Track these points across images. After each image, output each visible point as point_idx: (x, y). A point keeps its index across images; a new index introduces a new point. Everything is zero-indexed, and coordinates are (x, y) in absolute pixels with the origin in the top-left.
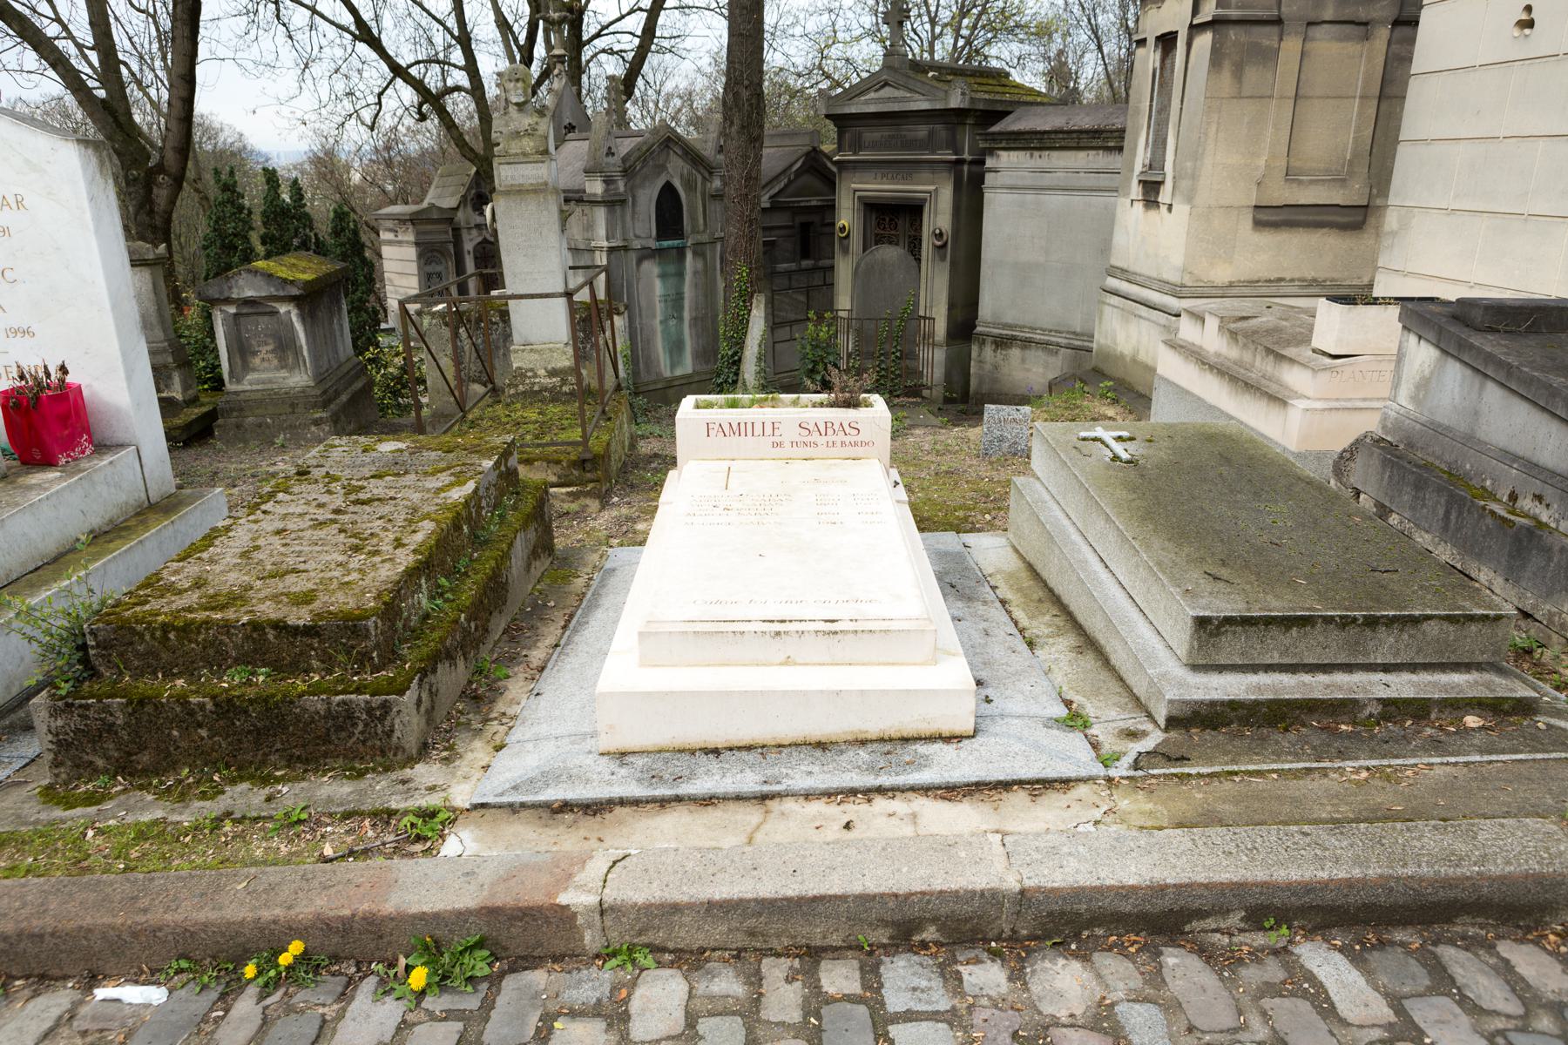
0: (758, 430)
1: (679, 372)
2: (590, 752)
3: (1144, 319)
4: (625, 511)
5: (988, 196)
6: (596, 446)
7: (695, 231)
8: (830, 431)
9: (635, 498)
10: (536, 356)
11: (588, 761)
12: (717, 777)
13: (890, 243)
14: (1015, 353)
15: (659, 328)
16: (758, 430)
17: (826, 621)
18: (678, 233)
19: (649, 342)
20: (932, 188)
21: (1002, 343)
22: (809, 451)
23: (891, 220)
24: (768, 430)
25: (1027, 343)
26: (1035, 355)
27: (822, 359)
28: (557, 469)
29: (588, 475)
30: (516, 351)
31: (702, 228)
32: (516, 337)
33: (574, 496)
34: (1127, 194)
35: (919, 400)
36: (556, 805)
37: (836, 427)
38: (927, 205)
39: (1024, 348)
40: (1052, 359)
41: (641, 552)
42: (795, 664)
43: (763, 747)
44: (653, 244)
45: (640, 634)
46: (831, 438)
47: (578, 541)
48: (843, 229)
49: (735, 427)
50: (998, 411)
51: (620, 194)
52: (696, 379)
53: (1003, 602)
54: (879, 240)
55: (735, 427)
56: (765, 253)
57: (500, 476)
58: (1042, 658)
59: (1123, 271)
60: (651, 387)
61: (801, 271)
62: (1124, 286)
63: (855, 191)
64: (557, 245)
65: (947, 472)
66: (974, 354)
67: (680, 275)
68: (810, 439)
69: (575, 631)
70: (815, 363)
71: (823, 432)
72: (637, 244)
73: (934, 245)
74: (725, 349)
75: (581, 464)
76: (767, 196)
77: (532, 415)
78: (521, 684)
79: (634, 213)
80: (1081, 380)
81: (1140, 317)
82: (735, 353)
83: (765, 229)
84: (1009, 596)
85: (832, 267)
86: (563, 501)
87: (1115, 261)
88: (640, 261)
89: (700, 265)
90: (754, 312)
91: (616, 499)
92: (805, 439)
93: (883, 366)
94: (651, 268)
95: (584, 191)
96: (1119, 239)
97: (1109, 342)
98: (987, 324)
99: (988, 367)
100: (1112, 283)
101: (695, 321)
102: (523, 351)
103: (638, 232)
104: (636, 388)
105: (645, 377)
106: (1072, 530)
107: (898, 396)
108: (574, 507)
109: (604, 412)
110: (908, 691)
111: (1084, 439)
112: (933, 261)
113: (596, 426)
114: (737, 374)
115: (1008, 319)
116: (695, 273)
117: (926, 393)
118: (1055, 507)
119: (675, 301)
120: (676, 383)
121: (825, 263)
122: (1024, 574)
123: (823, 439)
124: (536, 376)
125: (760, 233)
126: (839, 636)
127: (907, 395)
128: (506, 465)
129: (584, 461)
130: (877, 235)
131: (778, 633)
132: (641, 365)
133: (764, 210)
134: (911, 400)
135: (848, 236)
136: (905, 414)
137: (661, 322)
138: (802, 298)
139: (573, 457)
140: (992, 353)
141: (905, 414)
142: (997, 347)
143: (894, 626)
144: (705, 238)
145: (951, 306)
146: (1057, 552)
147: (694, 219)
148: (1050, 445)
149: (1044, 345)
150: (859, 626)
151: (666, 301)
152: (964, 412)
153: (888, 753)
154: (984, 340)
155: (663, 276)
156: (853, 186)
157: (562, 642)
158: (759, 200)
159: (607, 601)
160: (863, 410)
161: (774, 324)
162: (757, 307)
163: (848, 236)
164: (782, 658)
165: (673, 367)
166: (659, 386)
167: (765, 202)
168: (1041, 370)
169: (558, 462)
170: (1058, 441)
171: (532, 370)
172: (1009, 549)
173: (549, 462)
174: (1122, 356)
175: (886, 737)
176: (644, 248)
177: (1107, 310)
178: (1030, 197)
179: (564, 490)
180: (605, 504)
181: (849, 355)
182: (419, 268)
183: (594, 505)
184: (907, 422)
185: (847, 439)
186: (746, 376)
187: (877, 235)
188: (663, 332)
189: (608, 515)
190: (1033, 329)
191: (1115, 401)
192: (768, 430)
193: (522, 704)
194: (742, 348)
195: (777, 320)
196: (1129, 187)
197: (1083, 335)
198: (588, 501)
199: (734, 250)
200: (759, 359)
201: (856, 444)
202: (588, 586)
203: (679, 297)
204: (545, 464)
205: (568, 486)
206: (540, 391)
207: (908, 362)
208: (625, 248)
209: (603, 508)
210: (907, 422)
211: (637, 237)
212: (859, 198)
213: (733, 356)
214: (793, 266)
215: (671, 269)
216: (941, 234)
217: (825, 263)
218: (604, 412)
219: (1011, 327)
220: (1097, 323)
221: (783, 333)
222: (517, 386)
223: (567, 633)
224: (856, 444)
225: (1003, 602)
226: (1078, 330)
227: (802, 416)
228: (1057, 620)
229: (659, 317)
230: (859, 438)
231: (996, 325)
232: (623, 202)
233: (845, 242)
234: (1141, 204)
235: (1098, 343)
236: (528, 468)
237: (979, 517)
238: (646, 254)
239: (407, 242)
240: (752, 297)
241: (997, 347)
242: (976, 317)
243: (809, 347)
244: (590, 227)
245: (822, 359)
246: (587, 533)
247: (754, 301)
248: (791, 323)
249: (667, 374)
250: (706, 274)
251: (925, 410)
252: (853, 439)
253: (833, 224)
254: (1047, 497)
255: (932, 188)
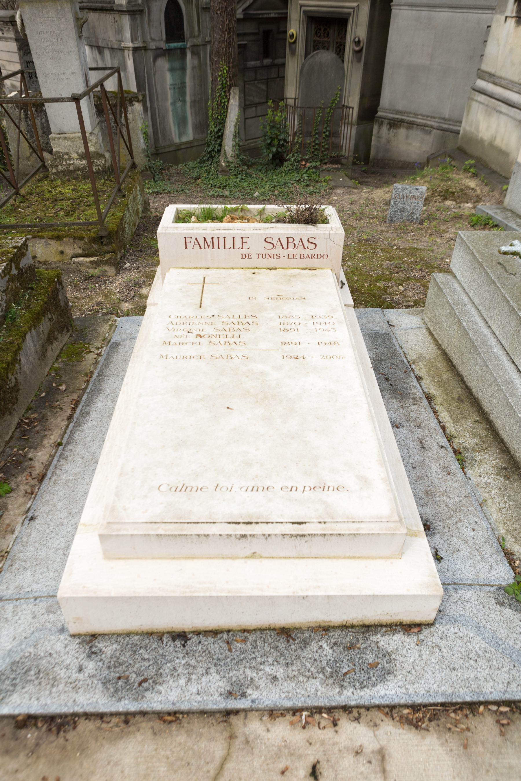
0: (229, 243)
1: (184, 139)
2: (62, 630)
3: (504, 114)
4: (134, 275)
5: (394, 12)
6: (111, 223)
7: (192, 36)
8: (291, 245)
9: (143, 262)
10: (69, 143)
11: (59, 646)
12: (182, 681)
13: (324, 48)
14: (402, 131)
15: (170, 108)
16: (229, 243)
17: (293, 523)
18: (181, 38)
19: (164, 118)
20: (355, 4)
21: (394, 124)
22: (273, 262)
23: (325, 30)
24: (238, 244)
25: (411, 125)
26: (416, 134)
27: (277, 136)
28: (81, 244)
29: (106, 248)
30: (54, 139)
31: (197, 33)
32: (53, 128)
33: (96, 264)
34: (503, 12)
35: (339, 166)
36: (20, 718)
37: (297, 242)
38: (351, 18)
39: (408, 128)
40: (427, 137)
41: (139, 324)
42: (261, 557)
43: (229, 631)
44: (164, 45)
45: (101, 536)
46: (291, 251)
47: (98, 304)
48: (292, 36)
49: (209, 240)
50: (403, 189)
51: (138, 5)
52: (196, 144)
53: (429, 398)
54: (316, 47)
55: (209, 240)
56: (239, 53)
57: (12, 279)
58: (475, 480)
59: (491, 75)
60: (167, 150)
61: (263, 67)
62: (490, 87)
63: (301, 6)
64: (76, 50)
65: (367, 240)
66: (375, 131)
67: (183, 69)
68: (273, 251)
69: (78, 424)
70: (272, 139)
71: (285, 246)
72: (153, 45)
73: (353, 49)
74: (213, 128)
75: (99, 239)
76: (241, 10)
77: (68, 191)
78: (21, 500)
79: (149, 21)
80: (450, 156)
81: (501, 112)
82: (219, 130)
83: (239, 35)
84: (433, 391)
85: (284, 65)
86: (88, 267)
87: (484, 67)
88: (155, 59)
89: (196, 62)
90: (232, 101)
91: (128, 265)
92: (270, 252)
93: (317, 142)
94: (163, 64)
95: (114, 3)
96: (491, 49)
97: (473, 130)
98: (385, 110)
99: (383, 140)
100: (481, 84)
101: (193, 102)
102: (59, 138)
103: (153, 36)
104: (157, 150)
105: (162, 143)
106: (492, 341)
107: (326, 163)
108: (96, 272)
109: (120, 190)
110: (374, 596)
111: (505, 253)
112: (352, 62)
113: (113, 203)
114: (220, 145)
115: (400, 107)
116: (193, 68)
117: (344, 161)
118: (474, 312)
119: (180, 89)
120: (183, 147)
121: (279, 61)
122: (441, 364)
123: (286, 252)
124: (70, 158)
125: (236, 39)
126: (306, 538)
127: (332, 163)
128: (17, 268)
129: (101, 237)
130: (315, 41)
131: (244, 536)
132: (160, 135)
133: (239, 20)
134: (334, 166)
135: (295, 42)
136: (330, 177)
137: (172, 104)
138: (264, 87)
139: (93, 235)
140: (387, 132)
141: (330, 177)
142: (391, 127)
143: (364, 529)
144: (199, 41)
145: (362, 97)
146: (480, 361)
147: (191, 27)
148: (475, 257)
149: (422, 127)
150: (328, 529)
151: (174, 88)
152: (365, 172)
153: (351, 647)
154: (382, 122)
155: (172, 70)
156: (300, 2)
157: (65, 440)
158: (235, 13)
159: (107, 385)
160: (320, 226)
161: (245, 106)
162: (234, 97)
163: (295, 42)
164: (249, 552)
165: (180, 135)
166: (172, 149)
167: (239, 15)
168: (418, 144)
169: (81, 238)
170: (483, 255)
171: (67, 154)
172: (425, 331)
173: (74, 238)
174: (482, 141)
175: (348, 624)
176: (158, 49)
177: (475, 105)
178: (424, 13)
179: (88, 259)
180: (119, 269)
181: (295, 134)
182: (20, 58)
183: (111, 271)
184: (332, 183)
185: (306, 252)
186: (227, 148)
187: (315, 41)
188: (173, 111)
189: (122, 278)
190: (416, 115)
191: (475, 176)
192: (238, 244)
193: (16, 533)
194: (223, 127)
195: (247, 103)
196: (505, 6)
197: (449, 120)
198: (106, 268)
199: (218, 52)
200: (235, 136)
201: (313, 256)
202: (96, 363)
203: (183, 85)
204: (71, 240)
205: (92, 256)
206: (75, 171)
207: (333, 138)
208: (145, 48)
209: (118, 272)
210: (332, 183)
211: (153, 39)
212: (304, 12)
213: (218, 132)
214: (257, 63)
215: (177, 64)
216: (359, 42)
217: (279, 61)
218: (120, 190)
219: (398, 112)
220: (465, 114)
221: (251, 112)
222: (57, 166)
223: (72, 425)
224: (313, 256)
225: (429, 398)
226: (447, 116)
227: (267, 231)
228: (479, 427)
229: (170, 101)
230: (315, 252)
231: (391, 111)
232: (141, 12)
233: (293, 46)
234: (513, 20)
235: (464, 129)
236: (59, 243)
237: (395, 288)
238: (160, 53)
239: (10, 38)
240: (230, 89)
241: (391, 127)
242: (378, 105)
243: (268, 127)
244: (119, 31)
245: (277, 136)
246: (106, 295)
247: (231, 91)
248: (256, 105)
249: (177, 140)
250: (200, 67)
251: (342, 174)
252: (310, 252)
253: (285, 32)
254: (466, 300)
255: (355, 4)
